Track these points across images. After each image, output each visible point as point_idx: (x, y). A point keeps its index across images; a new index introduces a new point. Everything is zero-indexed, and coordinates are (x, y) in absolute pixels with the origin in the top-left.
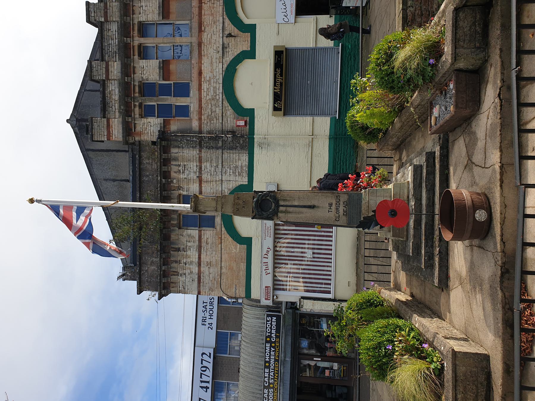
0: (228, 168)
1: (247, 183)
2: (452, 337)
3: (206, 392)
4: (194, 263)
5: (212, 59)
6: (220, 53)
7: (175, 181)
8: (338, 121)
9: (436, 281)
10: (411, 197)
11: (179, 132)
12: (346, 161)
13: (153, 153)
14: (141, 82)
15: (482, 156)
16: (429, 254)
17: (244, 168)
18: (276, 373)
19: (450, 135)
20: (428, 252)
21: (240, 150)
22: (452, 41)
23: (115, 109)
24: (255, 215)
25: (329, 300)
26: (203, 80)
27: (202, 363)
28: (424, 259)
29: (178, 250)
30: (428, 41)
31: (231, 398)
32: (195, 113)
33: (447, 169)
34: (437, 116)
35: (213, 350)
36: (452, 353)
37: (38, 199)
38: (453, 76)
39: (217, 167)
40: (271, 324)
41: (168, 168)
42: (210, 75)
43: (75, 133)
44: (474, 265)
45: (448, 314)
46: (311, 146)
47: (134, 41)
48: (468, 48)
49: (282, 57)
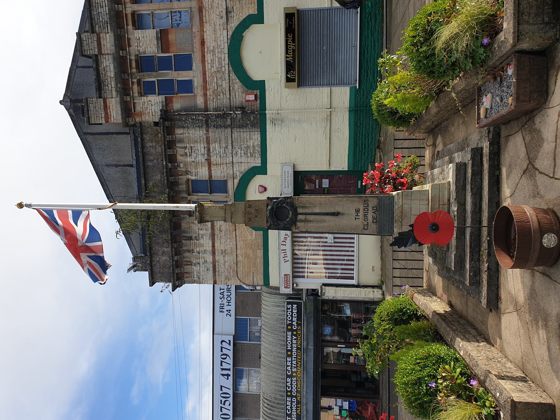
0: (238, 148)
1: (260, 165)
2: (508, 377)
3: (228, 379)
4: (208, 252)
5: (215, 25)
6: (223, 19)
7: (182, 165)
8: (359, 90)
9: (484, 301)
10: (452, 200)
11: (183, 110)
12: (369, 135)
13: (156, 135)
14: (138, 55)
15: (550, 163)
16: (474, 269)
17: (257, 148)
18: (299, 362)
19: (503, 128)
20: (474, 267)
21: (251, 128)
22: (514, 15)
23: (112, 87)
24: (270, 226)
25: (353, 286)
26: (206, 50)
27: (222, 351)
28: (470, 275)
29: (190, 238)
30: (482, 13)
31: (253, 384)
32: (200, 88)
33: (498, 170)
34: (488, 107)
35: (232, 336)
36: (512, 405)
37: (28, 203)
38: (514, 60)
39: (227, 148)
40: (292, 312)
41: (173, 151)
42: (214, 44)
43: (70, 115)
44: (536, 294)
45: (498, 340)
46: (329, 120)
47: (127, 9)
48: (535, 24)
49: (293, 20)
